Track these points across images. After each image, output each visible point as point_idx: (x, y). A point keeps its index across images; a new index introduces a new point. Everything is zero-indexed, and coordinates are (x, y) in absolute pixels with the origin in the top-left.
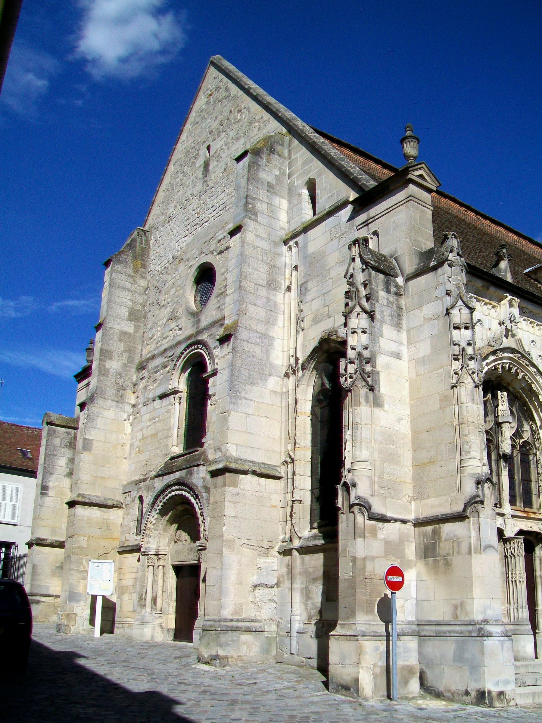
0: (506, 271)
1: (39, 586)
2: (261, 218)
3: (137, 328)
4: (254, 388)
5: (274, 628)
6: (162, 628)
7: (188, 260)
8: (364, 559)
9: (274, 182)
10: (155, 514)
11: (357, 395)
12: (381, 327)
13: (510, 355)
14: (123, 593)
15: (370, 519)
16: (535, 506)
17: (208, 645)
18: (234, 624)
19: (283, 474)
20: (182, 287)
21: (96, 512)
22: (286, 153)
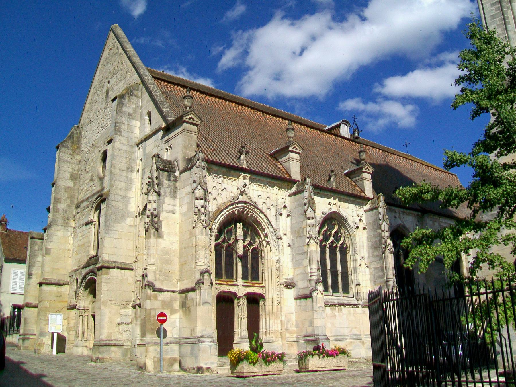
0: (243, 160)
1: (29, 330)
2: (124, 133)
3: (75, 184)
4: (119, 224)
5: (129, 344)
6: (87, 347)
7: (99, 147)
8: (150, 309)
9: (132, 112)
10: (82, 288)
11: (150, 233)
12: (164, 199)
13: (243, 205)
14: (69, 331)
15: (153, 291)
16: (260, 279)
17: (95, 353)
18: (108, 342)
19: (134, 267)
20: (95, 162)
21: (54, 288)
22: (140, 94)
